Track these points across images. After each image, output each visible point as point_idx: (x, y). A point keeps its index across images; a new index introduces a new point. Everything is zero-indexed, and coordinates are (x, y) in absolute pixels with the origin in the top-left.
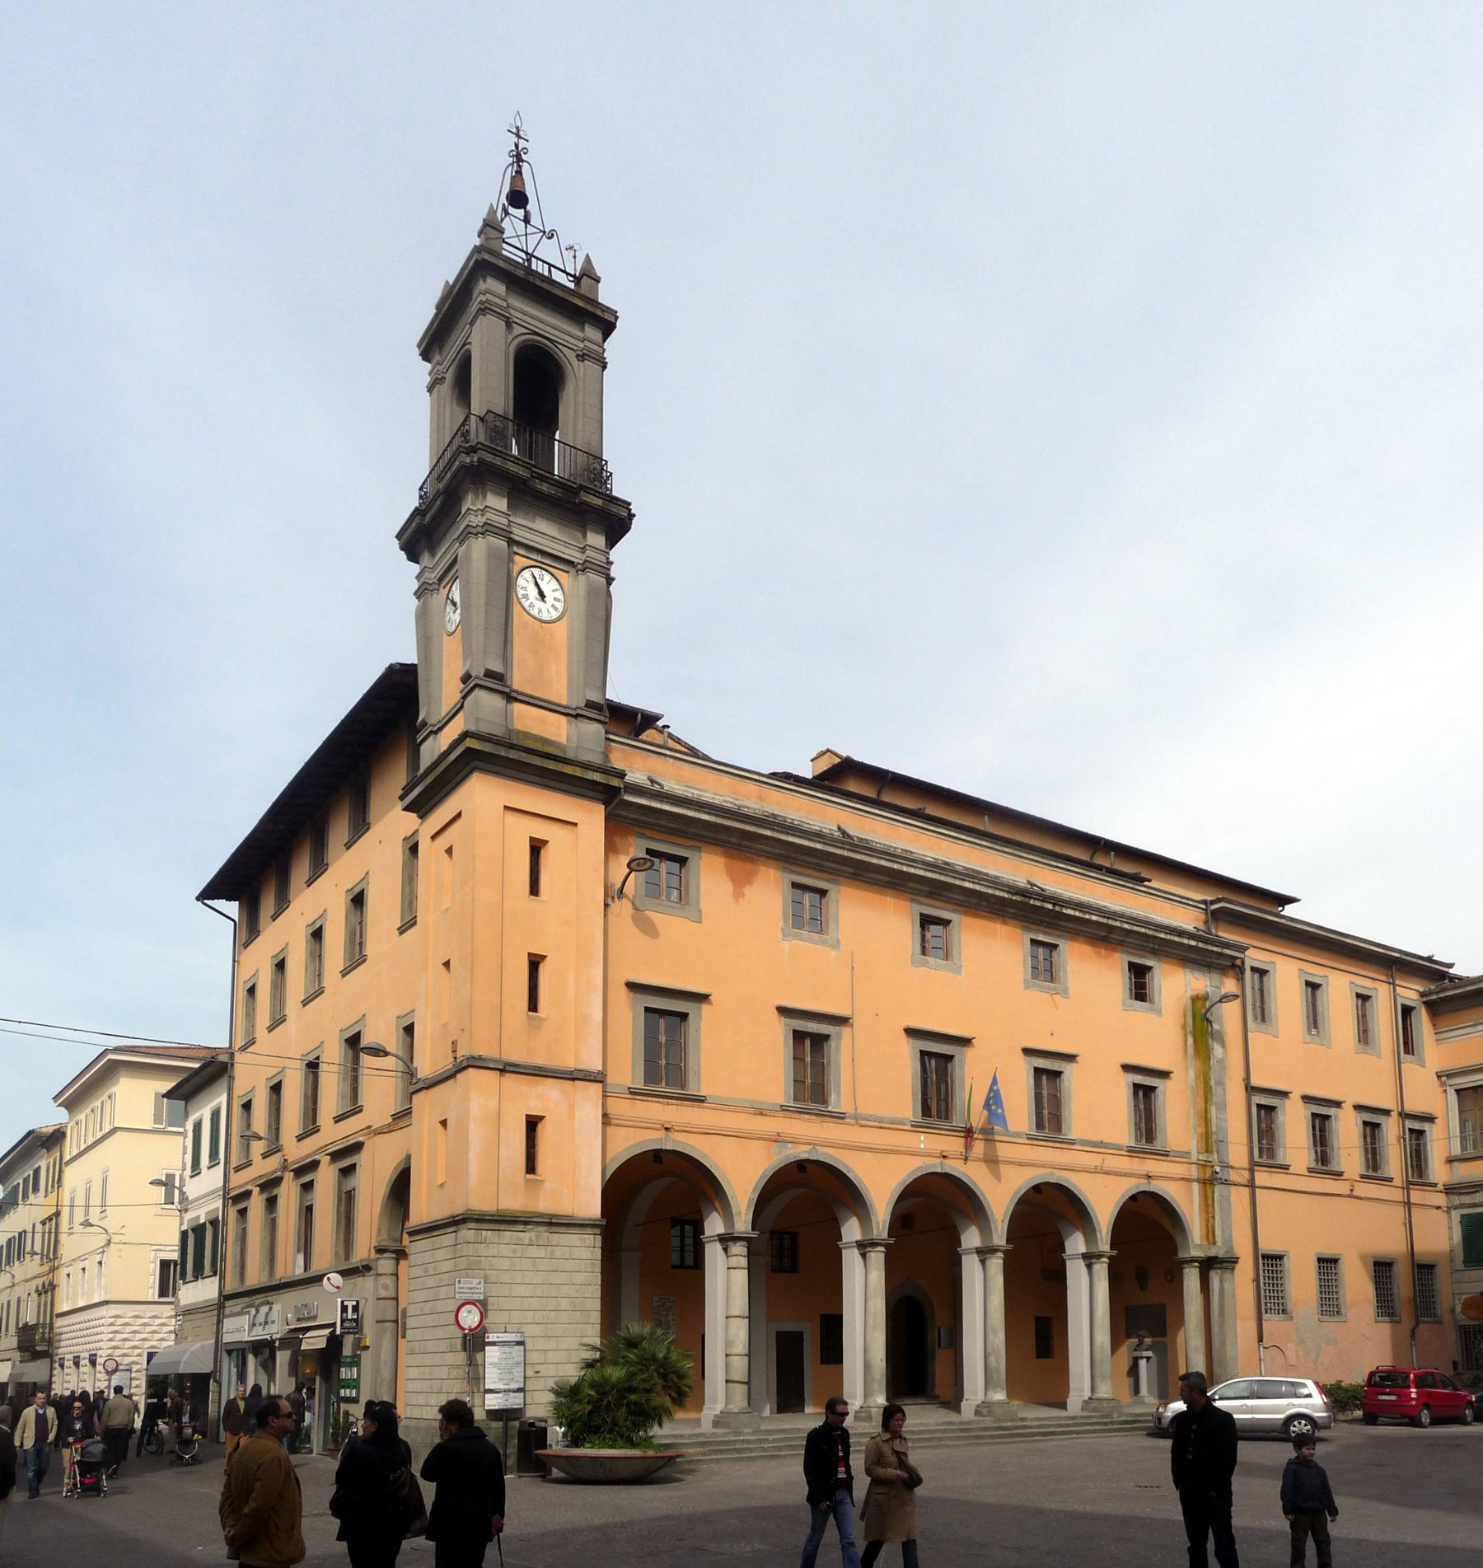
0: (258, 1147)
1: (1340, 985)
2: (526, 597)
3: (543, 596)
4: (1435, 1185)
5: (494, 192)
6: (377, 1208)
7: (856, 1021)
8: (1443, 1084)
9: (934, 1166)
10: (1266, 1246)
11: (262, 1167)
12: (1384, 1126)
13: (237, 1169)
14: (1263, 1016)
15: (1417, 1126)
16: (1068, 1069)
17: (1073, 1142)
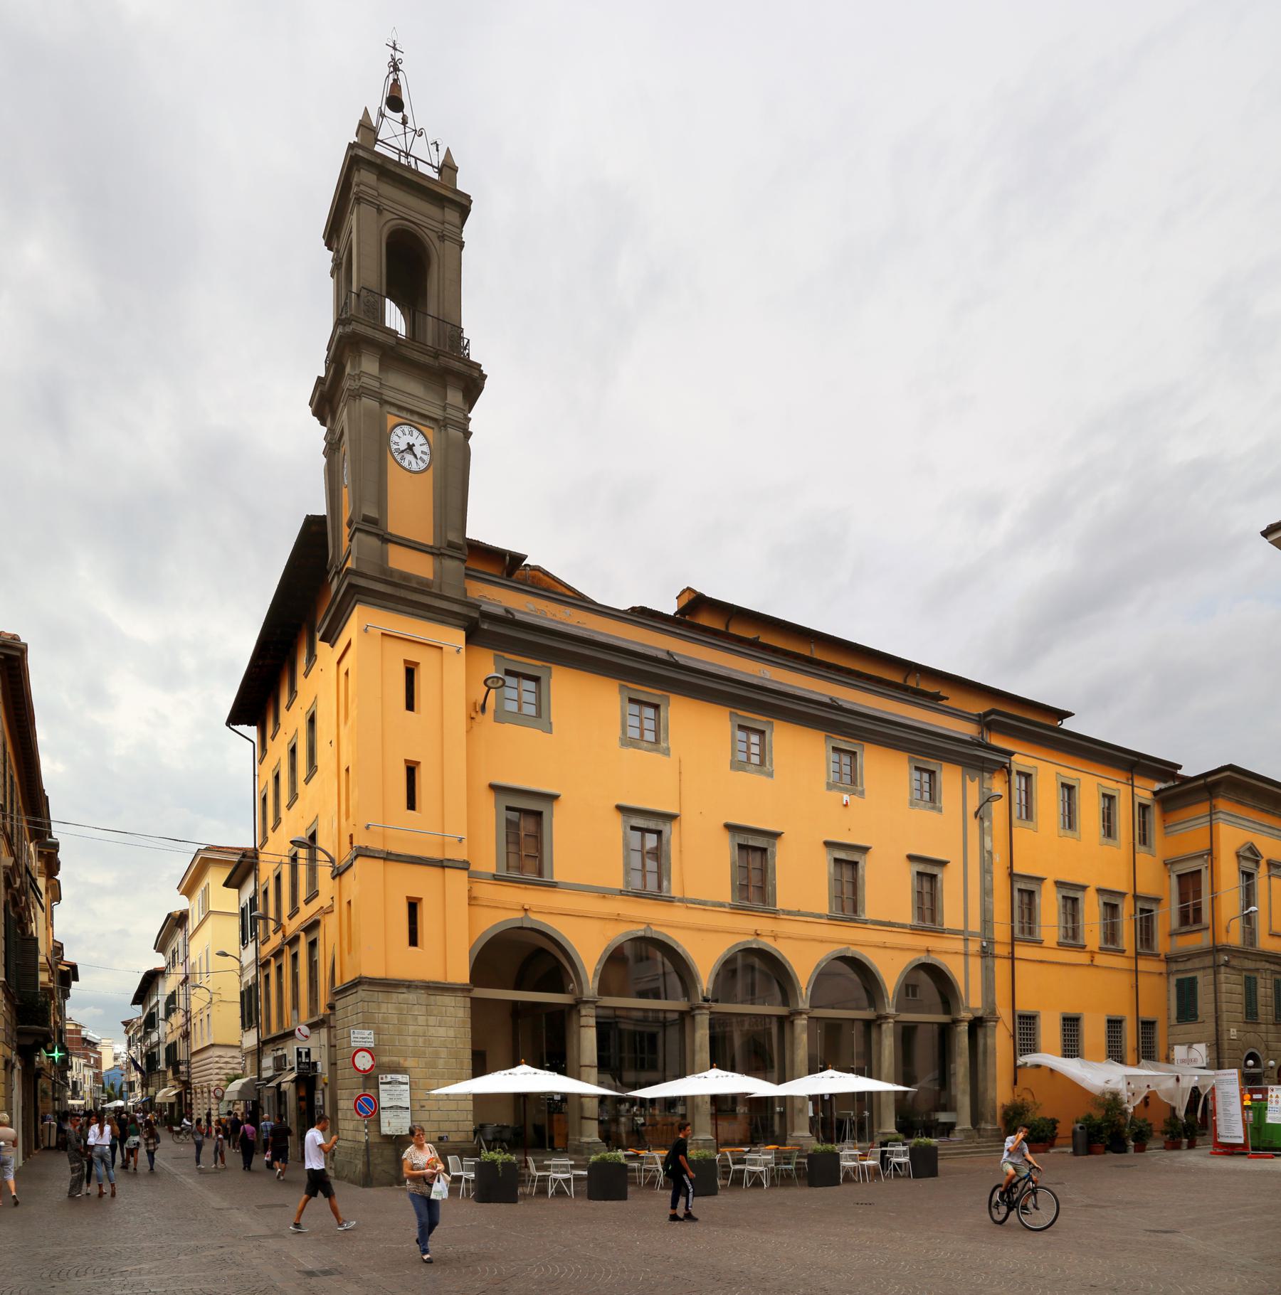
0: (272, 925)
1: (1092, 784)
4: (1158, 955)
5: (375, 100)
7: (683, 817)
8: (1169, 871)
10: (1022, 1007)
11: (276, 940)
12: (940, 876)
13: (263, 943)
14: (1029, 816)
15: (1071, 894)
17: (866, 922)
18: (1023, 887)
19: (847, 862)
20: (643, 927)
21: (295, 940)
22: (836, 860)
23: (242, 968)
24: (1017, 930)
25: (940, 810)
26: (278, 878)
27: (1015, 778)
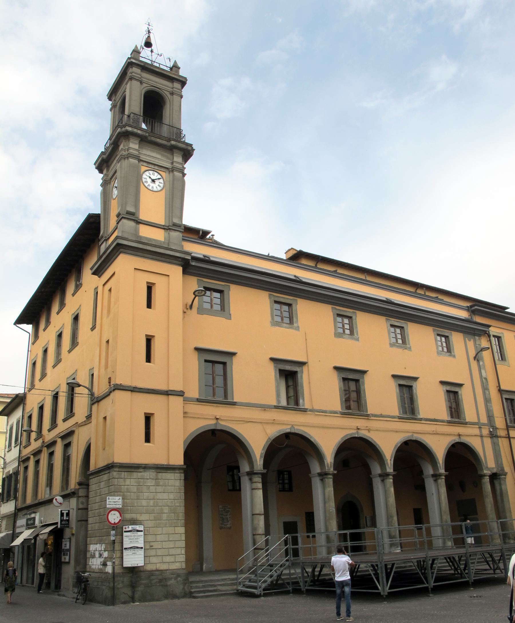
0: (33, 435)
2: (146, 182)
3: (153, 182)
6: (79, 463)
7: (310, 363)
9: (355, 434)
11: (35, 445)
12: (460, 392)
13: (25, 447)
14: (503, 358)
17: (421, 419)
18: (507, 397)
19: (406, 386)
20: (289, 427)
21: (53, 443)
22: (400, 385)
23: (5, 463)
24: (508, 422)
25: (454, 356)
26: (41, 408)
27: (493, 339)
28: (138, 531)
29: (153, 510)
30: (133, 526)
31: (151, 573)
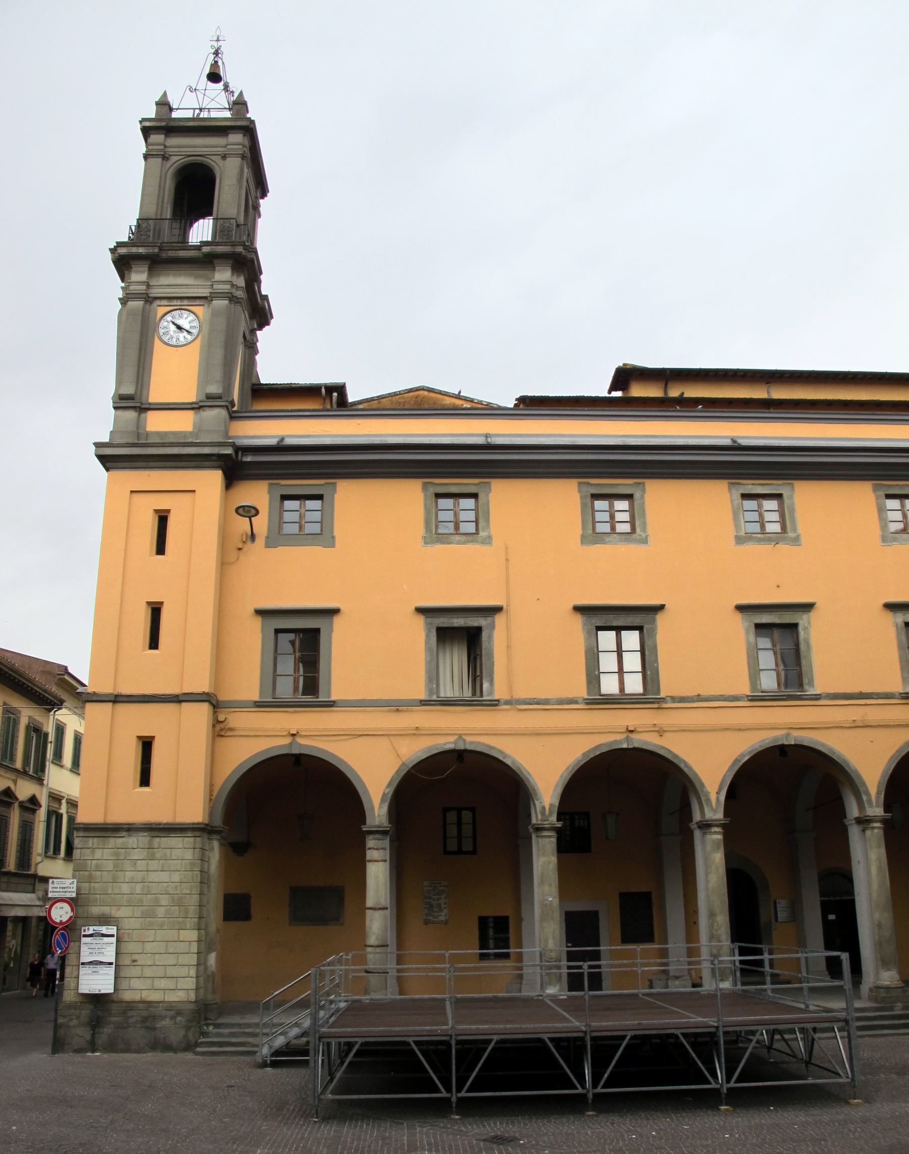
9: (620, 742)
16: (802, 620)
17: (817, 697)
20: (452, 739)
28: (104, 935)
29: (141, 901)
30: (96, 928)
31: (130, 1006)
